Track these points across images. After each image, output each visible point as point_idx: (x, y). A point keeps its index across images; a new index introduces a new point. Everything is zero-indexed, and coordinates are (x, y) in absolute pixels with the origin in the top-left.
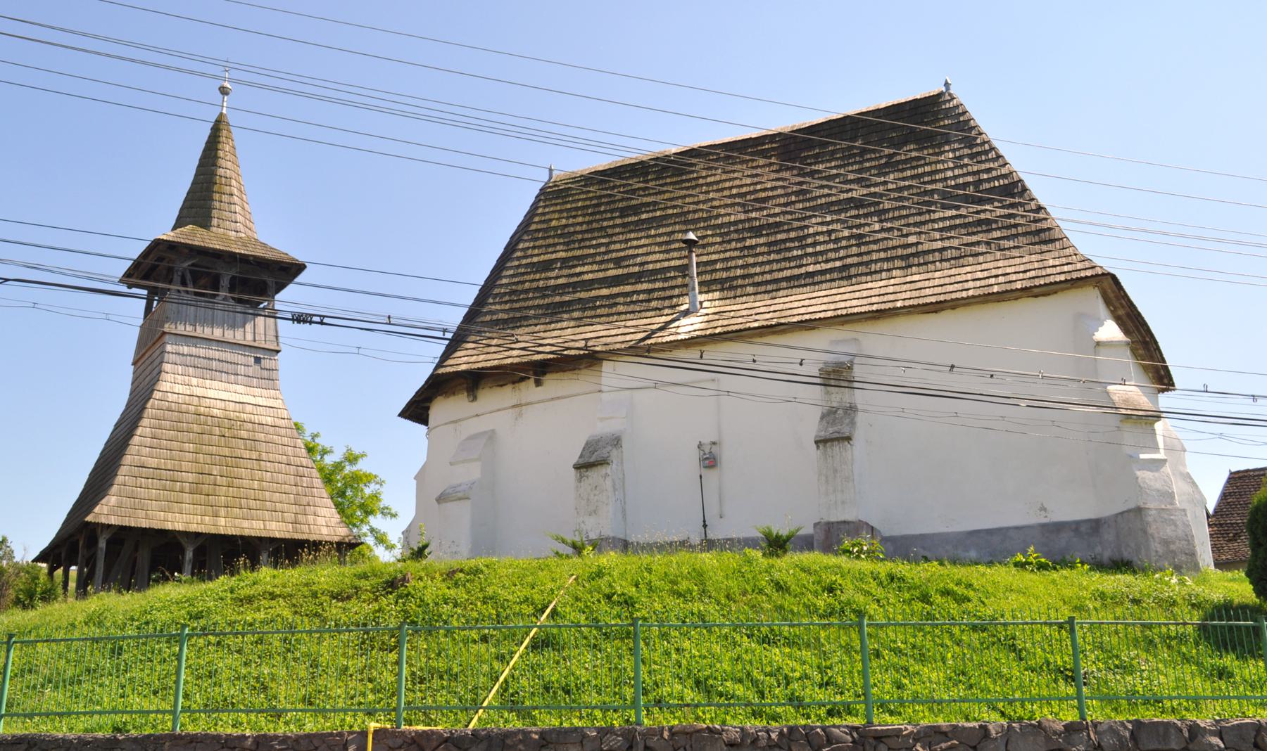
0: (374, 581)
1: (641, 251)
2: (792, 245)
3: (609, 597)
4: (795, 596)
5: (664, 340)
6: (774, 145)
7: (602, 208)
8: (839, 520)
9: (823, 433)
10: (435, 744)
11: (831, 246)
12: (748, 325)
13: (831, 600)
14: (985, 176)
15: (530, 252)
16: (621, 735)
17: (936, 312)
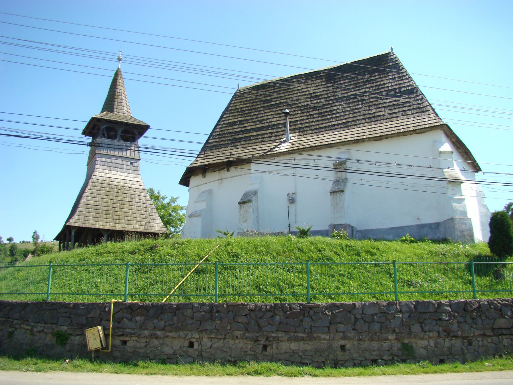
0: (145, 247)
1: (270, 117)
2: (327, 114)
3: (229, 253)
4: (305, 253)
7: (257, 100)
8: (338, 224)
9: (333, 189)
10: (136, 308)
11: (342, 114)
13: (320, 255)
14: (403, 86)
15: (228, 118)
16: (208, 306)
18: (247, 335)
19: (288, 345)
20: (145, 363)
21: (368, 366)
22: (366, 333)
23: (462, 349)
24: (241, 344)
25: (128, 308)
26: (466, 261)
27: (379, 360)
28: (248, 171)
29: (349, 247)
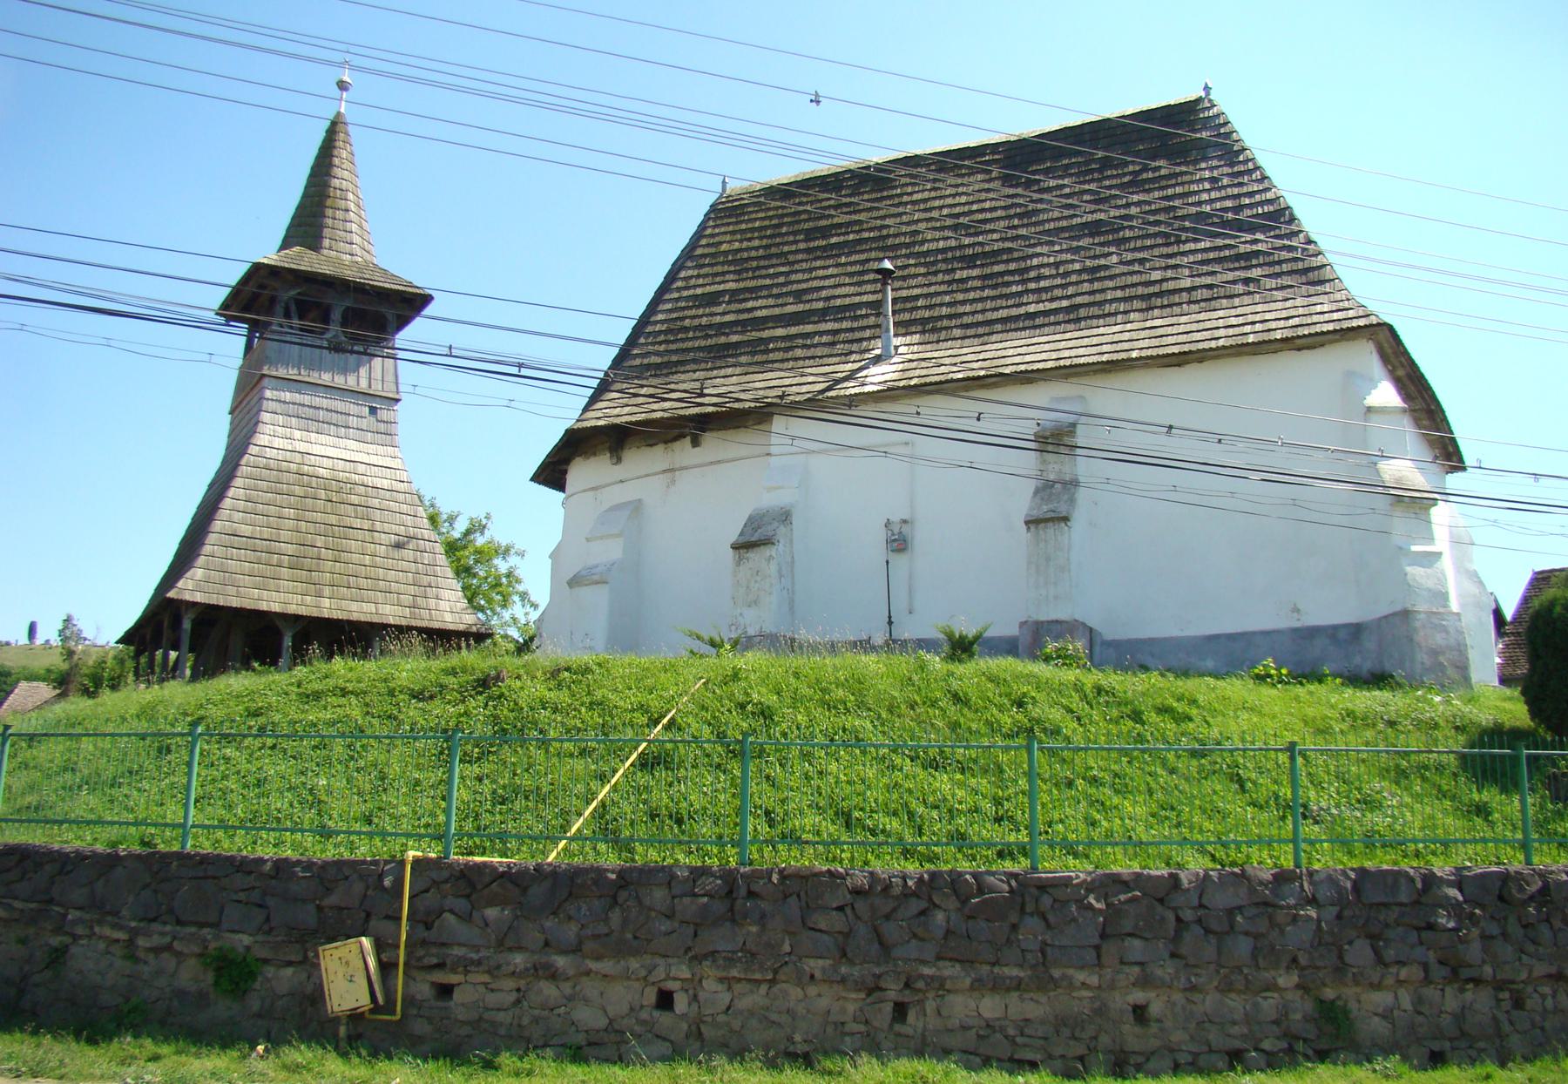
0: (463, 678)
1: (827, 283)
2: (1011, 279)
3: (742, 706)
5: (848, 392)
6: (996, 157)
7: (784, 230)
8: (1050, 619)
10: (487, 879)
11: (1059, 281)
12: (951, 376)
13: (1020, 717)
14: (1247, 201)
15: (693, 282)
16: (720, 878)
17: (1179, 365)
18: (844, 970)
19: (973, 1005)
20: (521, 1058)
21: (1219, 1072)
22: (1212, 967)
23: (1495, 1018)
24: (824, 999)
25: (458, 879)
26: (1458, 743)
27: (1248, 1051)
28: (764, 450)
29: (1107, 692)
